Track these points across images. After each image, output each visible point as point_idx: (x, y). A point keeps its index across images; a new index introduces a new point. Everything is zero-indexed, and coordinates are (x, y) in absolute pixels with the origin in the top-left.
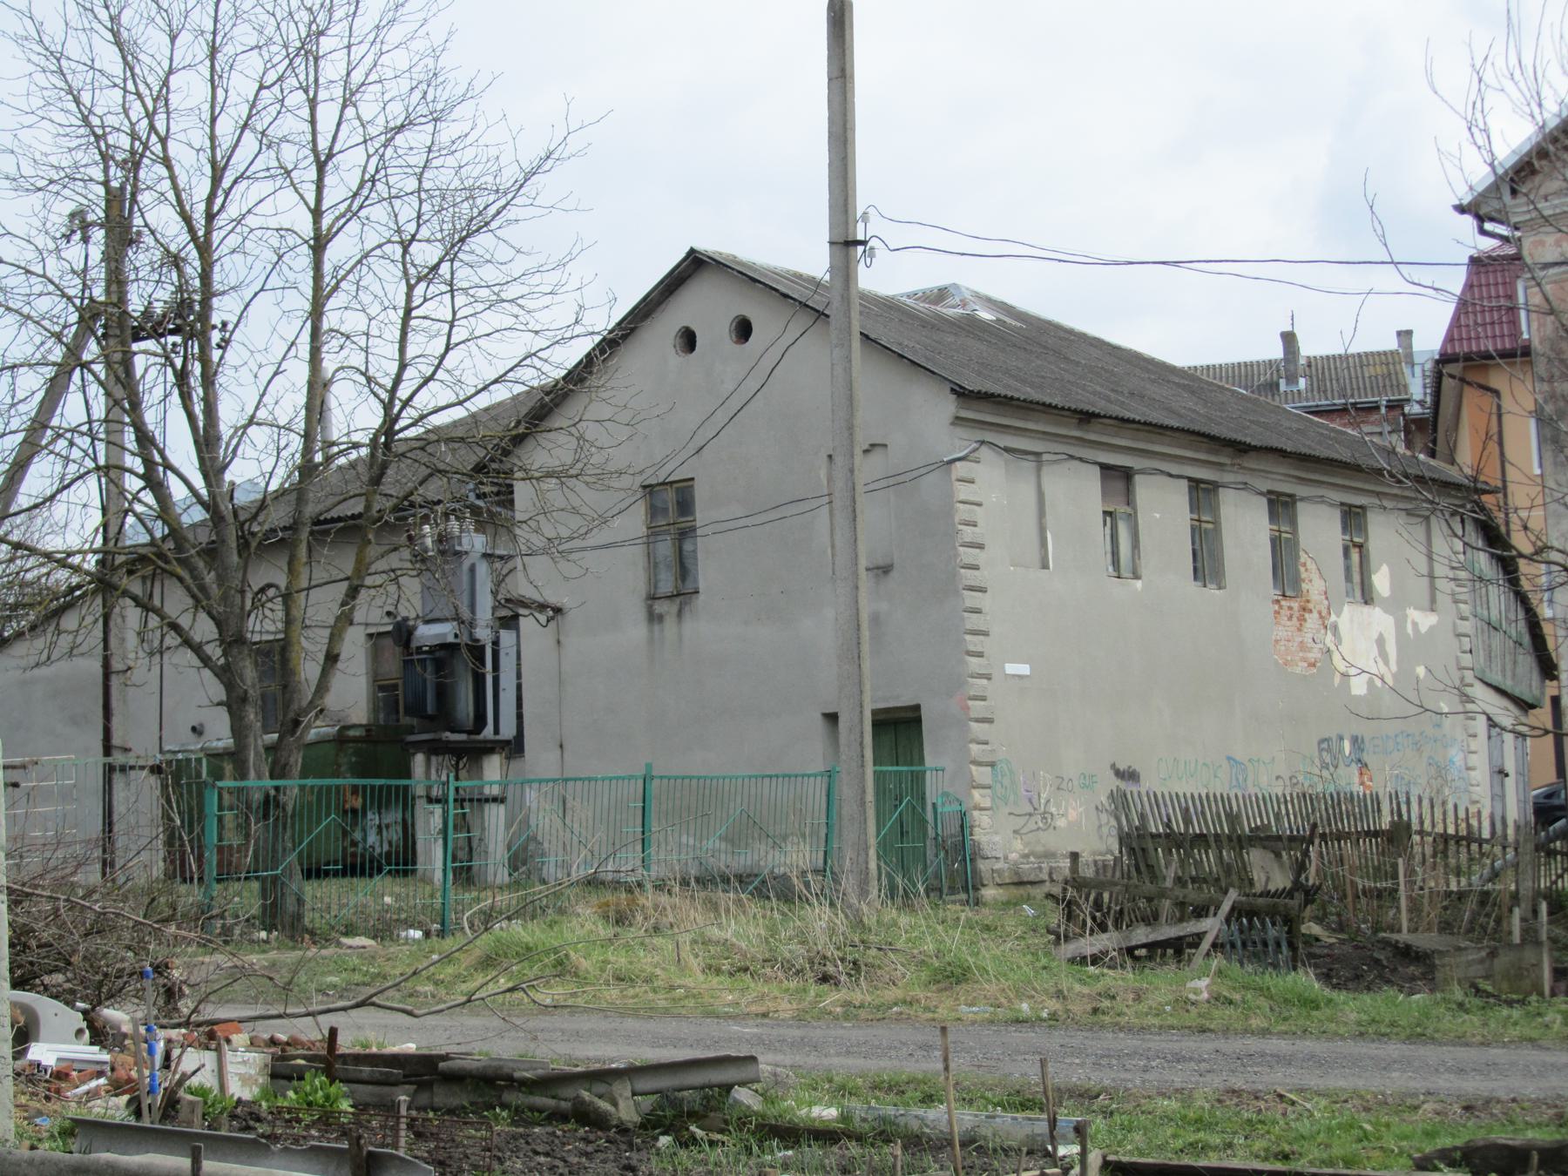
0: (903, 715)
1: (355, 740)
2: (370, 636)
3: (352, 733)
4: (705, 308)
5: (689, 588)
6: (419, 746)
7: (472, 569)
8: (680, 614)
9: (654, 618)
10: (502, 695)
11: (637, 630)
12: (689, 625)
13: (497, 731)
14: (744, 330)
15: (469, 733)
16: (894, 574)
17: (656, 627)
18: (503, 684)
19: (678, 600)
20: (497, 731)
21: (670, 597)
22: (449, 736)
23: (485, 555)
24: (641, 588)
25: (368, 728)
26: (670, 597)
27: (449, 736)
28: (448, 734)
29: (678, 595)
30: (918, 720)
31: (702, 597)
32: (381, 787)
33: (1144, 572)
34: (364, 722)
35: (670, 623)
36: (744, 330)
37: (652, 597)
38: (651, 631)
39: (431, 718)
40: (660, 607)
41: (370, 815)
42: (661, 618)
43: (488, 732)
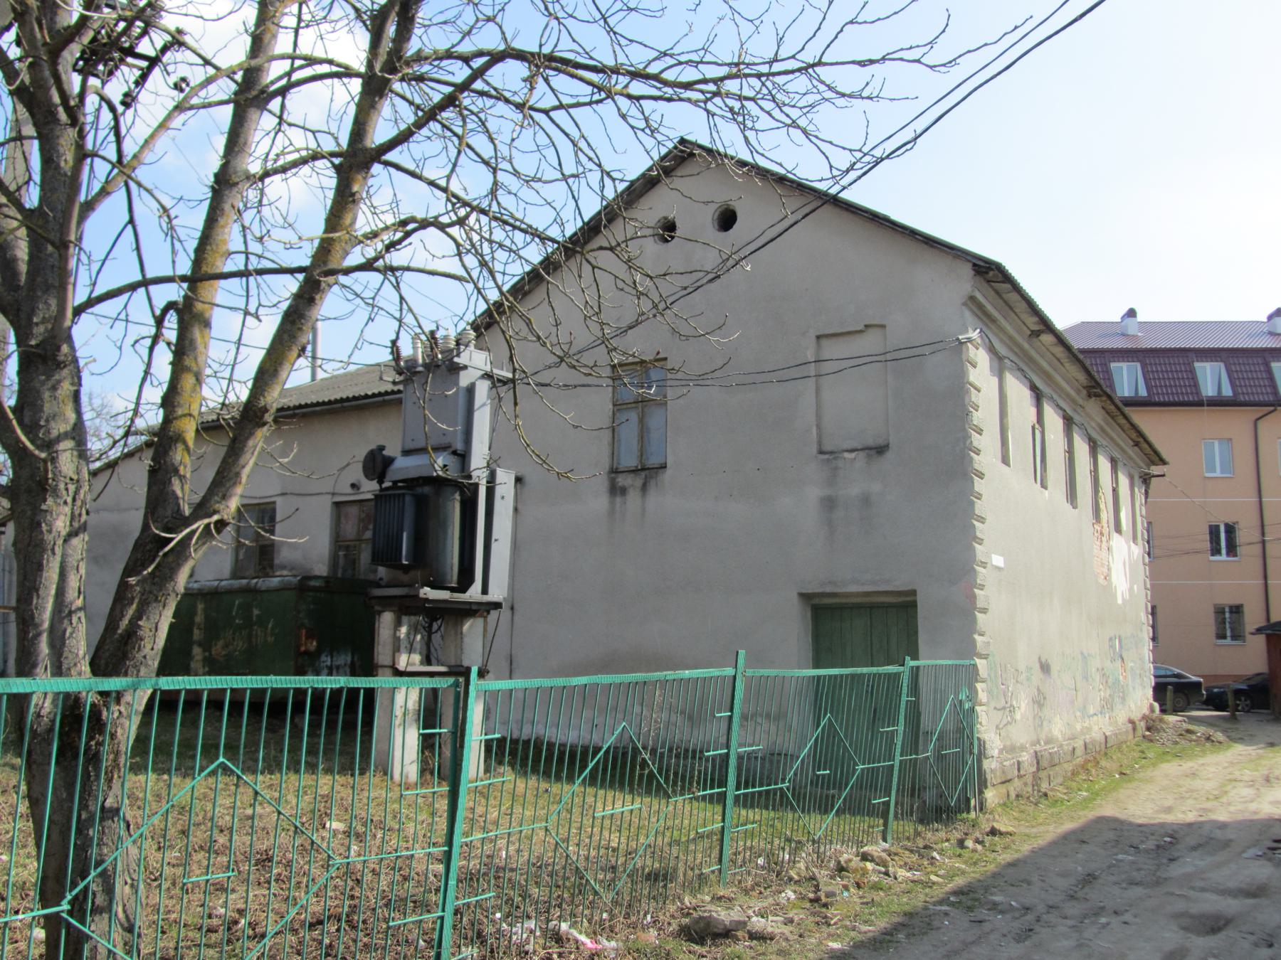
0: (859, 600)
1: (315, 589)
2: (338, 505)
3: (312, 583)
4: (686, 201)
5: (654, 461)
6: (387, 603)
7: (471, 390)
8: (644, 488)
9: (616, 490)
10: (494, 546)
11: (598, 501)
12: (653, 498)
13: (485, 591)
14: (727, 220)
15: (453, 590)
16: (889, 455)
17: (618, 500)
18: (496, 533)
19: (643, 474)
20: (485, 591)
21: (635, 471)
22: (427, 592)
23: (488, 376)
24: (605, 463)
25: (326, 579)
26: (635, 471)
27: (427, 592)
28: (427, 589)
29: (643, 469)
30: (914, 605)
31: (669, 472)
32: (336, 693)
33: (1050, 484)
34: (325, 574)
35: (633, 497)
36: (727, 220)
37: (614, 471)
38: (612, 503)
39: (406, 569)
40: (622, 480)
41: (323, 658)
42: (623, 491)
43: (474, 593)
